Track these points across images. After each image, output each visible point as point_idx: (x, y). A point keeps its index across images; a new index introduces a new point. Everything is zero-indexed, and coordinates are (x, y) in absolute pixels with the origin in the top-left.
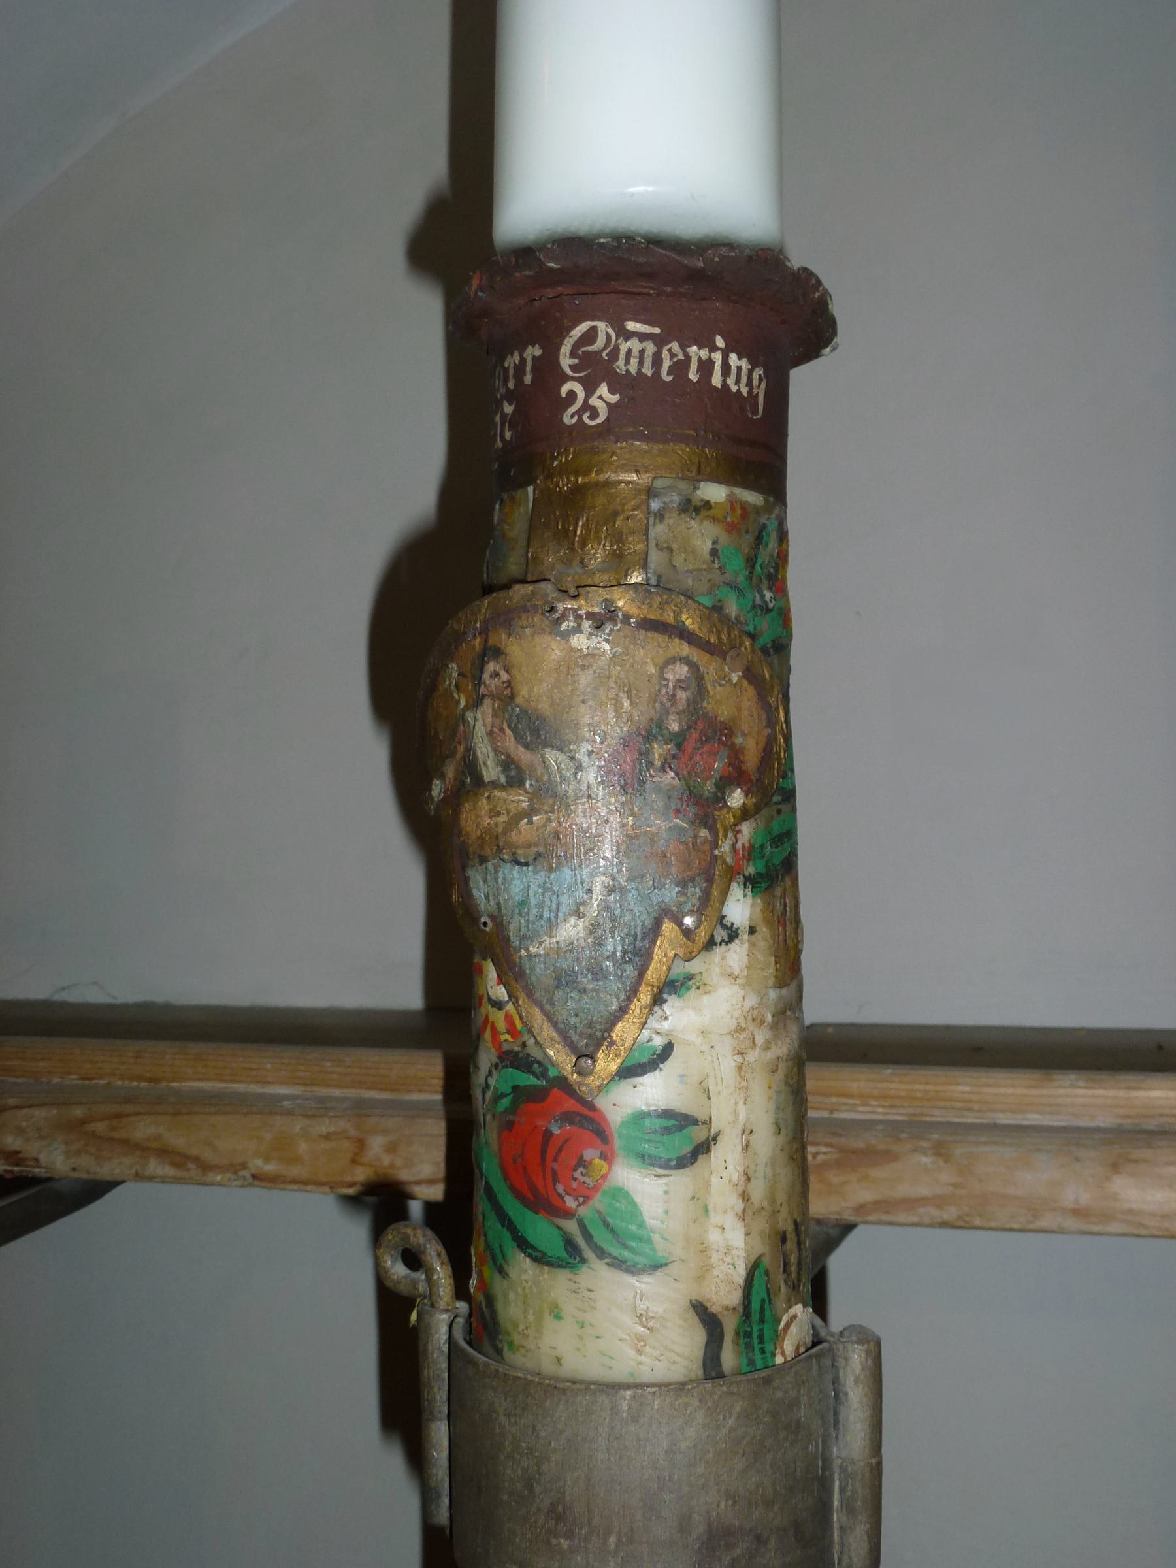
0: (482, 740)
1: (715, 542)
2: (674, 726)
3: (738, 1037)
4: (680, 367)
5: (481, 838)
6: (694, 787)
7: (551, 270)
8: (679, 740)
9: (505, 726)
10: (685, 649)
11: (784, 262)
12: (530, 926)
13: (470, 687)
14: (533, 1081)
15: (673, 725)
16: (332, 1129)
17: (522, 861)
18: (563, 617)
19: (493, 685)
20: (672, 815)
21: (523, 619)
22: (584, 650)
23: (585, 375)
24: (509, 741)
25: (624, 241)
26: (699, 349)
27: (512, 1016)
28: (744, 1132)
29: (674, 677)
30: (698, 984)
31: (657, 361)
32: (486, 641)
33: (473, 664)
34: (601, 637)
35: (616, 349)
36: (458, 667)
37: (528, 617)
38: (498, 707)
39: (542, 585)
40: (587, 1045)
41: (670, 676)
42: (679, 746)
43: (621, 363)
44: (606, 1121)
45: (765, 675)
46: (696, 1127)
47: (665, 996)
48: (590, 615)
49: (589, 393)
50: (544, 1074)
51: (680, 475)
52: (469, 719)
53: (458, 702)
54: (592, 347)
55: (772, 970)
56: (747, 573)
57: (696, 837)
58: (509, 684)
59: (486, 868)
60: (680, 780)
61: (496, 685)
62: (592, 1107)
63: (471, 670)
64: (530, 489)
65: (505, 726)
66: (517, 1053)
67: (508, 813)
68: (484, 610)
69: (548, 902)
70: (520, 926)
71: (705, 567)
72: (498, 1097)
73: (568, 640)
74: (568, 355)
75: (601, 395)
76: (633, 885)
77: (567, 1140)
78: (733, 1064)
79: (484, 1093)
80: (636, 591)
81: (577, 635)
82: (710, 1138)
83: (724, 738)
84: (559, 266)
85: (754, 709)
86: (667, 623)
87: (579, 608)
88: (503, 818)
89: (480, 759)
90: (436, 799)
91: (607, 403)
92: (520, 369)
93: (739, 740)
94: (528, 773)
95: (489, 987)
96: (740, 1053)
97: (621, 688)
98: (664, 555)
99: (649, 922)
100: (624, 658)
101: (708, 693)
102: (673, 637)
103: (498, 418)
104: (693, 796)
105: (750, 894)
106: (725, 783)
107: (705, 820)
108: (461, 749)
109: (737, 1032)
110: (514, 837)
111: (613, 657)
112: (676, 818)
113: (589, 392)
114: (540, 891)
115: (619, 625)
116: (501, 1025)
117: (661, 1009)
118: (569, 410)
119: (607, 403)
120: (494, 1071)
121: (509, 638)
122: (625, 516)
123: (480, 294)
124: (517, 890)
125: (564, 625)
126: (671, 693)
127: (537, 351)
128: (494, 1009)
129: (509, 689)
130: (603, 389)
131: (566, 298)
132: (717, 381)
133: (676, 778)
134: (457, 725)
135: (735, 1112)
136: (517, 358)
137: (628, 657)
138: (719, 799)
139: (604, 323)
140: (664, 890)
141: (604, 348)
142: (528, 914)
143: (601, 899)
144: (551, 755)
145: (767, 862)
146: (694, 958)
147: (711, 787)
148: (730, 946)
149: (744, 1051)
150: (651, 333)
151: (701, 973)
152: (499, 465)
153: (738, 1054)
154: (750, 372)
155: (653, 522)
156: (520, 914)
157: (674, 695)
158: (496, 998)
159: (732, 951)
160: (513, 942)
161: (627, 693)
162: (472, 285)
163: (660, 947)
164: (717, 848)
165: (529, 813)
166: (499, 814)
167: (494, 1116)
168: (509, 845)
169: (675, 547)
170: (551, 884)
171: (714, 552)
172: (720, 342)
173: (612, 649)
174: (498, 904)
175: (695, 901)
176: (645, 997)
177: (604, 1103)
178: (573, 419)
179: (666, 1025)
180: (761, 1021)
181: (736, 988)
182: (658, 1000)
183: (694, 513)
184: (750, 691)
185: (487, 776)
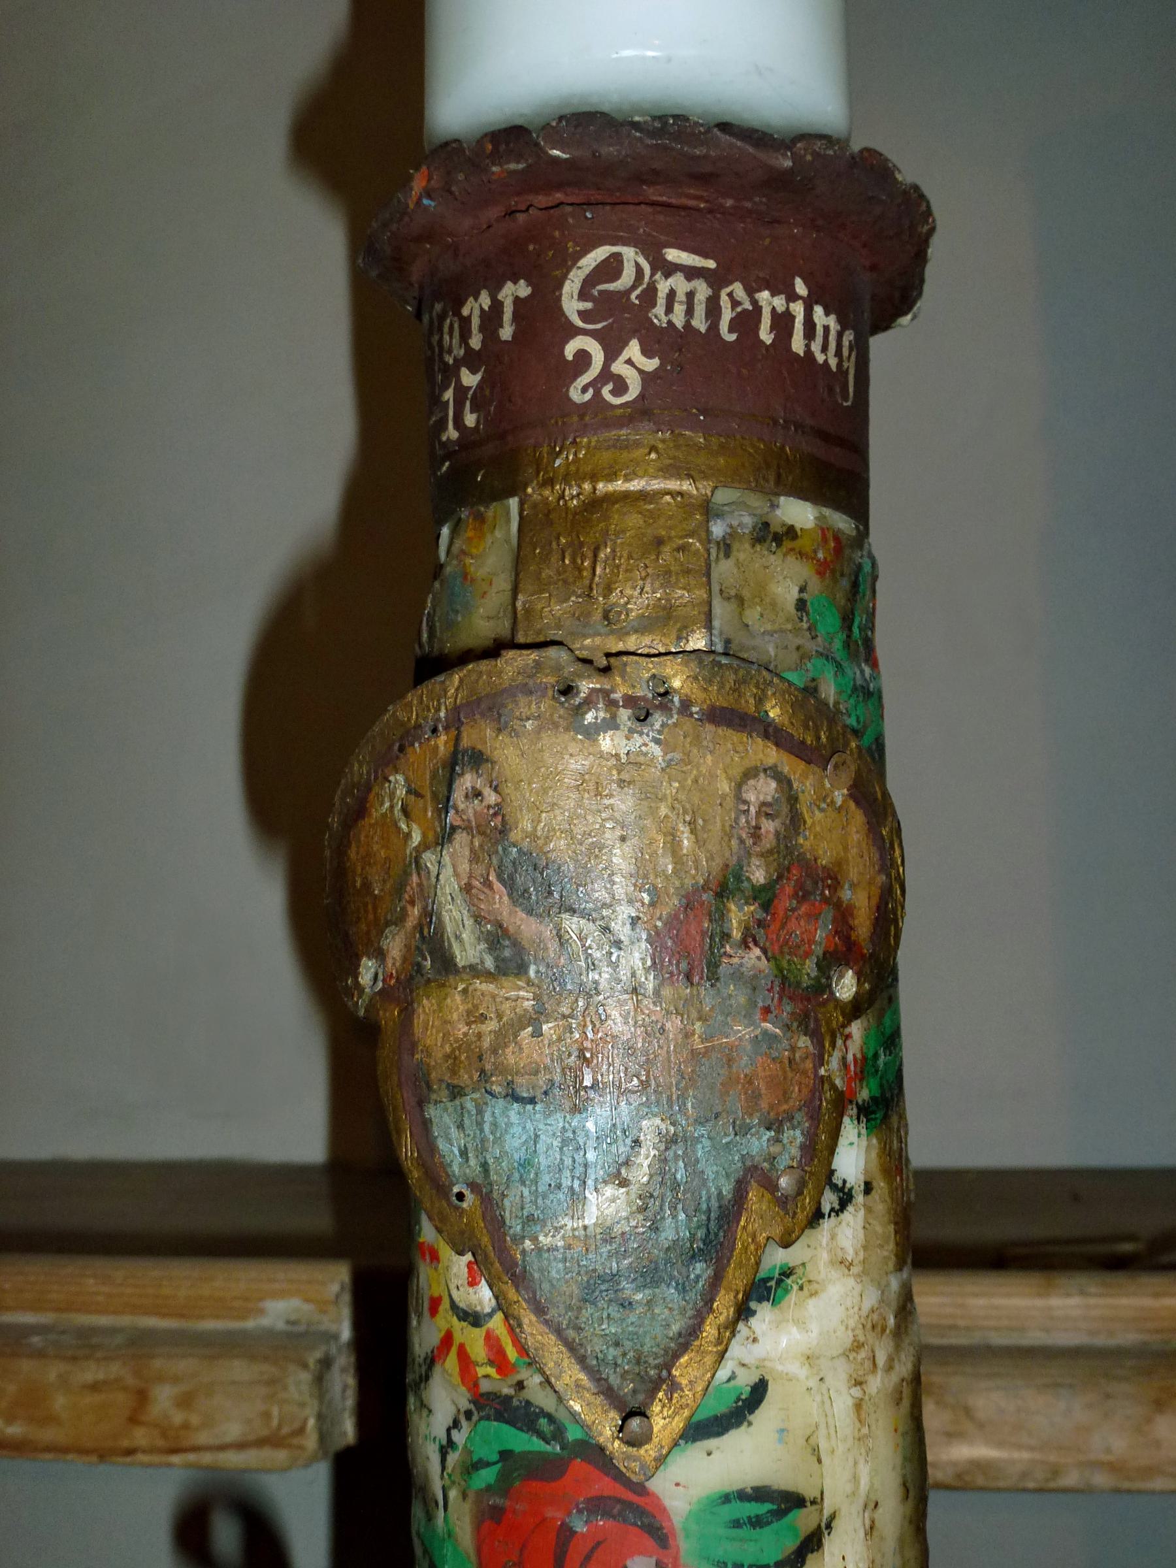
0: (452, 898)
1: (802, 590)
2: (759, 875)
3: (854, 1358)
4: (747, 322)
5: (452, 1057)
6: (789, 971)
7: (556, 160)
8: (765, 897)
9: (492, 878)
10: (772, 755)
11: (893, 173)
12: (540, 1201)
13: (430, 814)
14: (536, 1445)
15: (757, 874)
16: (101, 1376)
17: (525, 1095)
18: (588, 703)
19: (471, 812)
20: (758, 1016)
21: (521, 704)
22: (622, 755)
23: (603, 327)
24: (500, 902)
25: (671, 121)
26: (773, 295)
27: (498, 1339)
28: (866, 1506)
29: (758, 798)
30: (800, 1282)
31: (713, 310)
32: (458, 739)
33: (434, 776)
34: (648, 735)
35: (652, 290)
36: (407, 780)
37: (530, 703)
38: (481, 846)
39: (552, 652)
40: (634, 1391)
41: (751, 797)
42: (766, 907)
43: (660, 308)
44: (664, 1510)
45: (876, 792)
46: (804, 1510)
47: (753, 1305)
48: (630, 701)
49: (611, 355)
50: (558, 1434)
51: (753, 485)
52: (429, 865)
53: (408, 836)
54: (614, 284)
55: (891, 1246)
56: (845, 636)
57: (793, 1049)
58: (498, 811)
60: (768, 960)
61: (475, 813)
62: (641, 1489)
63: (431, 785)
64: (514, 503)
65: (492, 878)
66: (508, 1398)
67: (500, 1016)
68: (453, 691)
69: (568, 1162)
71: (789, 626)
72: (473, 1466)
73: (596, 740)
74: (576, 297)
76: (702, 1131)
77: (598, 1544)
78: (850, 1402)
79: (444, 1452)
80: (701, 662)
81: (610, 733)
82: (823, 1525)
83: (827, 892)
84: (568, 156)
85: (864, 845)
86: (746, 714)
87: (613, 691)
88: (492, 1025)
89: (449, 928)
90: (367, 990)
91: (640, 371)
92: (492, 318)
93: (846, 894)
95: (452, 1287)
96: (859, 1383)
97: (681, 816)
98: (732, 606)
99: (727, 1189)
100: (684, 769)
101: (805, 822)
102: (754, 735)
103: (449, 395)
104: (786, 984)
105: (864, 1131)
106: (831, 961)
107: (805, 1022)
108: (416, 911)
109: (854, 1350)
110: (510, 1056)
111: (667, 767)
112: (765, 1020)
113: (611, 354)
115: (676, 716)
116: (478, 1351)
117: (747, 1326)
118: (579, 379)
119: (640, 371)
120: (464, 1423)
121: (497, 736)
122: (675, 546)
123: (426, 202)
124: (517, 1143)
125: (589, 717)
126: (754, 823)
127: (523, 290)
128: (464, 1324)
129: (500, 818)
130: (633, 350)
131: (569, 209)
132: (798, 344)
133: (763, 958)
134: (406, 874)
135: (855, 1477)
136: (485, 300)
137: (689, 767)
138: (822, 987)
139: (633, 249)
140: (749, 1136)
141: (634, 287)
143: (655, 1156)
144: (572, 924)
145: (881, 1078)
146: (794, 1242)
147: (812, 970)
148: (842, 1216)
149: (862, 1379)
150: (703, 268)
151: (803, 1264)
152: (450, 465)
153: (855, 1385)
154: (840, 335)
155: (715, 556)
156: (523, 1183)
157: (758, 827)
158: (467, 1306)
159: (844, 1224)
161: (690, 823)
162: (411, 189)
163: (744, 1228)
164: (823, 1065)
165: (535, 1019)
166: (483, 1018)
167: (464, 1496)
168: (502, 1069)
169: (746, 594)
170: (574, 1132)
171: (801, 605)
172: (801, 288)
173: (666, 754)
174: (485, 1166)
175: (795, 1151)
176: (724, 1305)
177: (660, 1485)
178: (586, 395)
179: (759, 1351)
180: (882, 1327)
181: (851, 1282)
182: (743, 1312)
183: (774, 544)
184: (858, 818)
185: (462, 956)
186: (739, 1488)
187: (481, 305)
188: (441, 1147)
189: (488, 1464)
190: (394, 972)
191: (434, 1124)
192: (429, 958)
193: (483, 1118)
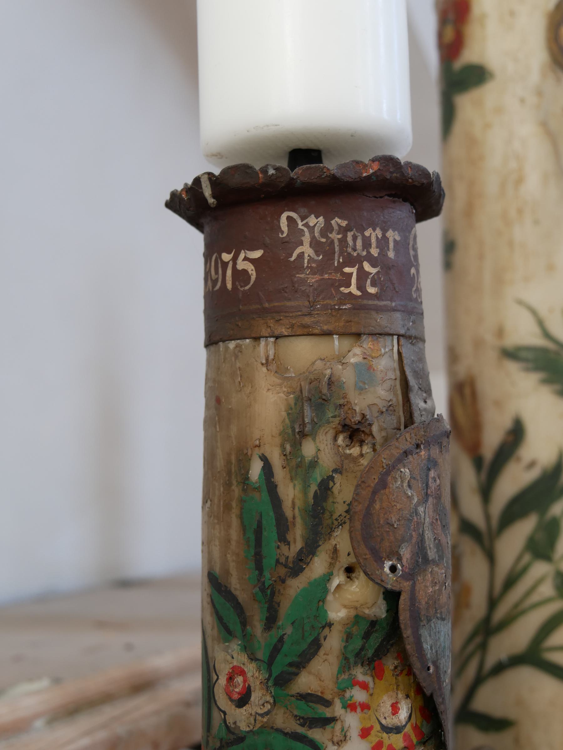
27: (409, 736)
187: (376, 234)
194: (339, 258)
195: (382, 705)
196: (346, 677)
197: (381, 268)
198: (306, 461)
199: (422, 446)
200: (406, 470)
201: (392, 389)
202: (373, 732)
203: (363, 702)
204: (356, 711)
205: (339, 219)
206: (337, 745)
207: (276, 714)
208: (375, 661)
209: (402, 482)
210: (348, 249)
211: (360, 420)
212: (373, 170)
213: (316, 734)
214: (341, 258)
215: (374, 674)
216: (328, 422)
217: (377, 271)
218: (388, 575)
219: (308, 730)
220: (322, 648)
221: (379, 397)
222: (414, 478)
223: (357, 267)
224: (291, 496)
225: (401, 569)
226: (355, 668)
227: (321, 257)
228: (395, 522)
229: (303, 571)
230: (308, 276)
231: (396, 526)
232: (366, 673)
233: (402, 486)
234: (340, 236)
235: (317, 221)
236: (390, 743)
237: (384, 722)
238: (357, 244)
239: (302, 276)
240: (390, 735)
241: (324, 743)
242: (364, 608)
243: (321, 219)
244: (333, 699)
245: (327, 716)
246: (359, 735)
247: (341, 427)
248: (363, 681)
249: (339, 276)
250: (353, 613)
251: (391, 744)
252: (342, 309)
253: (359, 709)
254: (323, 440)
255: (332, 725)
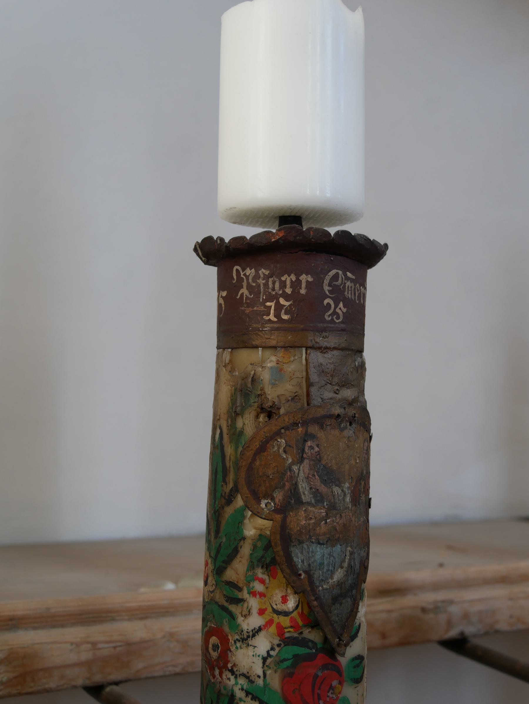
0: (303, 481)
12: (324, 575)
23: (334, 296)
27: (295, 619)
54: (337, 283)
59: (302, 546)
67: (316, 518)
70: (319, 575)
75: (340, 308)
88: (313, 521)
89: (301, 490)
94: (325, 498)
114: (328, 557)
130: (341, 305)
142: (323, 569)
160: (316, 583)
185: (304, 499)
186: (358, 654)
187: (291, 279)
188: (294, 560)
189: (288, 660)
190: (279, 504)
191: (293, 553)
192: (293, 500)
193: (309, 550)
194: (263, 296)
195: (274, 595)
196: (251, 574)
197: (294, 302)
198: (237, 431)
199: (300, 425)
200: (282, 440)
201: (299, 385)
202: (266, 612)
203: (261, 592)
204: (256, 597)
205: (264, 270)
206: (244, 617)
207: (216, 593)
208: (271, 566)
209: (279, 448)
210: (269, 290)
211: (271, 405)
212: (279, 236)
213: (233, 608)
214: (264, 296)
215: (269, 574)
216: (251, 406)
217: (290, 304)
218: (263, 509)
219: (229, 605)
220: (239, 553)
221: (287, 390)
222: (290, 446)
223: (275, 302)
224: (229, 453)
225: (274, 506)
226: (257, 569)
227: (252, 296)
228: (271, 474)
229: (232, 502)
230: (245, 309)
231: (271, 477)
232: (264, 573)
233: (279, 451)
234: (264, 281)
235: (250, 271)
236: (279, 622)
237: (275, 607)
238: (275, 286)
239: (243, 308)
240: (279, 616)
241: (236, 615)
242: (266, 530)
243: (253, 270)
244: (243, 587)
245: (239, 598)
246: (257, 613)
247: (260, 409)
248: (261, 578)
249: (263, 308)
250: (258, 532)
251: (280, 622)
252: (263, 330)
253: (258, 596)
254: (247, 418)
255: (242, 604)
